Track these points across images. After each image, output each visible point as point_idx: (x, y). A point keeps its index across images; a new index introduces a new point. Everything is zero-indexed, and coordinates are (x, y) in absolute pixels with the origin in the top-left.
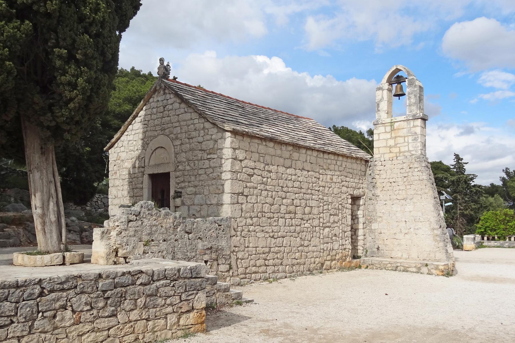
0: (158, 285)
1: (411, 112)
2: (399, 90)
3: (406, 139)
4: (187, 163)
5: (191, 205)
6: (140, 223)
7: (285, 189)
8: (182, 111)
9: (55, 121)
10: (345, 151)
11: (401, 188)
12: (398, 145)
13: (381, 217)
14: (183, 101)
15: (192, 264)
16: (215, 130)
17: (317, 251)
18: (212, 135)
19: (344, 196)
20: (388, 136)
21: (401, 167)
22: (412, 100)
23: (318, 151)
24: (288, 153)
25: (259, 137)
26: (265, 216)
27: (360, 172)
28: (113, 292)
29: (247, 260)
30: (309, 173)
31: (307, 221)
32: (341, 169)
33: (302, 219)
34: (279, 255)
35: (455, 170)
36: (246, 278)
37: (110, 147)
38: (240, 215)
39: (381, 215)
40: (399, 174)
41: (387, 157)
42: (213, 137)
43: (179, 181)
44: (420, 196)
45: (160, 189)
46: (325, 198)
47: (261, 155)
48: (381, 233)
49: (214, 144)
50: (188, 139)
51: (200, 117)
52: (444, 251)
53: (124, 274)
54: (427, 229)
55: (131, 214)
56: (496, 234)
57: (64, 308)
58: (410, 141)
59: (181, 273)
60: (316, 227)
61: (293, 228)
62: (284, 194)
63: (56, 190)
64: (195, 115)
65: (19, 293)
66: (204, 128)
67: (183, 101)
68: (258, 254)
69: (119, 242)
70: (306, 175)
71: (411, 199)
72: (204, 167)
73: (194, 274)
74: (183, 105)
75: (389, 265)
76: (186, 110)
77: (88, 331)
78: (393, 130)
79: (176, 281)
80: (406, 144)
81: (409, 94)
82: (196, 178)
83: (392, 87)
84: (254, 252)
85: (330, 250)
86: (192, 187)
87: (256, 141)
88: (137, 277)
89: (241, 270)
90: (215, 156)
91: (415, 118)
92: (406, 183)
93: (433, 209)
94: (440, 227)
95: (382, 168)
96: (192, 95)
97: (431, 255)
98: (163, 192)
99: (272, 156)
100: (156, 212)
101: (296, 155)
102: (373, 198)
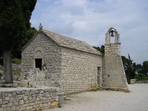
7: (78, 65)
10: (96, 53)
51: (52, 42)
56: (141, 79)
57: (22, 99)
87: (70, 50)
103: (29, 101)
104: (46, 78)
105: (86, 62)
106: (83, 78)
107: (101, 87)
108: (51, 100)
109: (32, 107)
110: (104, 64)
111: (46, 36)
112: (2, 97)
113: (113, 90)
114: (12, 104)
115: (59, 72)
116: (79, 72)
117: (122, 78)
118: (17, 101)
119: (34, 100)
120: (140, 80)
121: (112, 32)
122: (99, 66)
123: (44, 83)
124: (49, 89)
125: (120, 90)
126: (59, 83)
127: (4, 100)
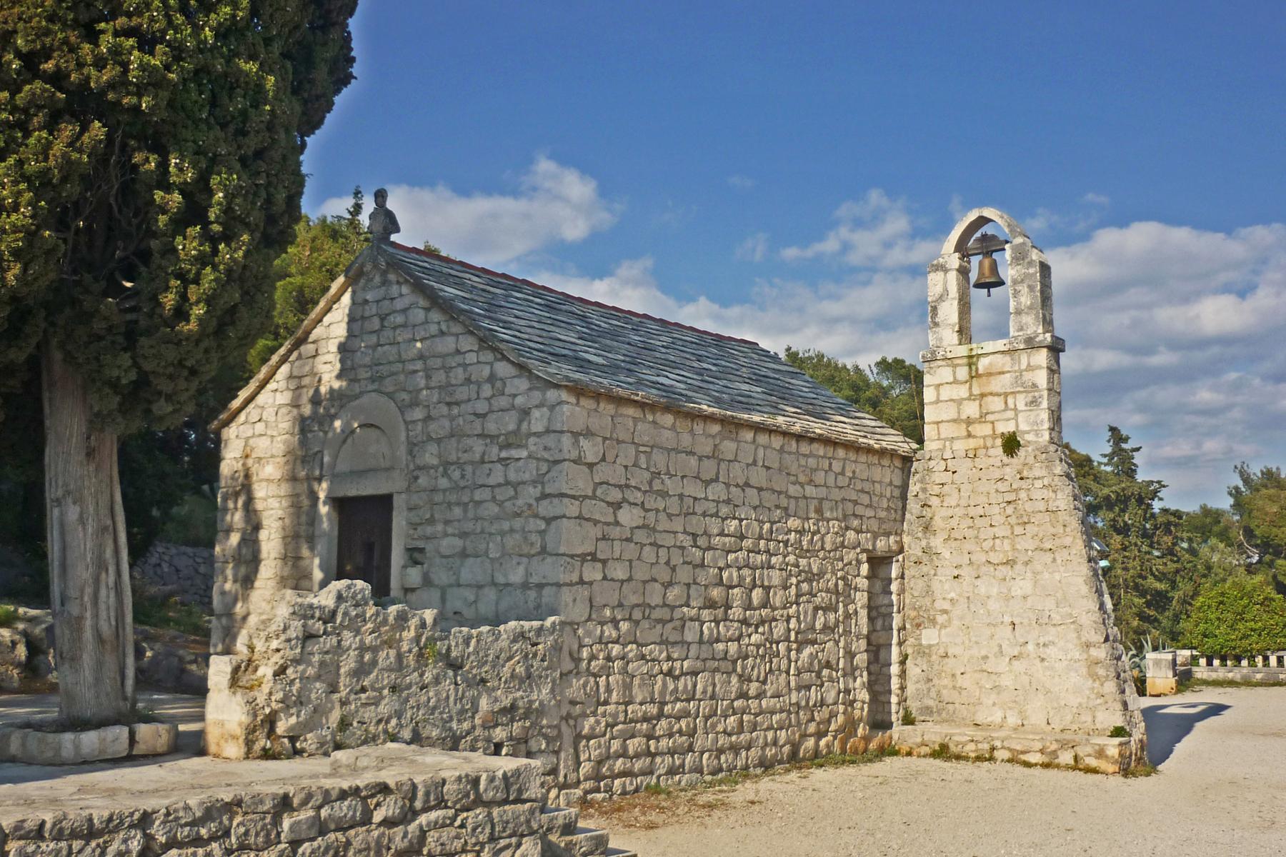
0: (424, 823)
1: (1021, 329)
2: (987, 271)
3: (1010, 401)
4: (441, 469)
5: (451, 586)
6: (335, 640)
8: (433, 329)
9: (139, 368)
11: (1000, 532)
12: (990, 418)
13: (945, 612)
14: (435, 301)
15: (505, 764)
16: (523, 384)
17: (782, 711)
18: (515, 396)
19: (850, 556)
20: (963, 392)
21: (998, 475)
22: (1023, 299)
24: (710, 441)
25: (636, 401)
26: (649, 617)
27: (889, 489)
28: (315, 844)
29: (602, 740)
31: (757, 627)
32: (842, 481)
33: (744, 622)
34: (683, 723)
35: (1109, 469)
36: (598, 790)
37: (227, 423)
38: (586, 615)
39: (946, 606)
40: (993, 494)
41: (960, 446)
42: (519, 401)
43: (417, 520)
44: (1049, 554)
45: (361, 538)
46: (803, 562)
47: (642, 449)
48: (946, 656)
49: (521, 421)
50: (449, 404)
52: (1119, 706)
53: (343, 795)
54: (1070, 646)
58: (1021, 406)
59: (482, 787)
60: (778, 643)
61: (721, 646)
62: (698, 553)
63: (117, 551)
64: (468, 343)
65: (94, 851)
66: (492, 378)
67: (435, 301)
68: (632, 721)
69: (280, 695)
71: (1026, 563)
72: (491, 481)
73: (511, 789)
74: (435, 316)
75: (971, 746)
76: (444, 328)
78: (974, 376)
79: (468, 810)
80: (1010, 414)
81: (1015, 282)
82: (465, 511)
83: (969, 262)
84: (621, 718)
85: (815, 705)
86: (454, 535)
88: (375, 801)
89: (586, 768)
90: (524, 454)
91: (1031, 344)
92: (1013, 520)
93: (1085, 589)
94: (1107, 639)
95: (947, 477)
96: (460, 284)
97: (1083, 718)
98: (369, 548)
99: (669, 451)
100: (374, 609)
101: (728, 447)
102: (925, 559)
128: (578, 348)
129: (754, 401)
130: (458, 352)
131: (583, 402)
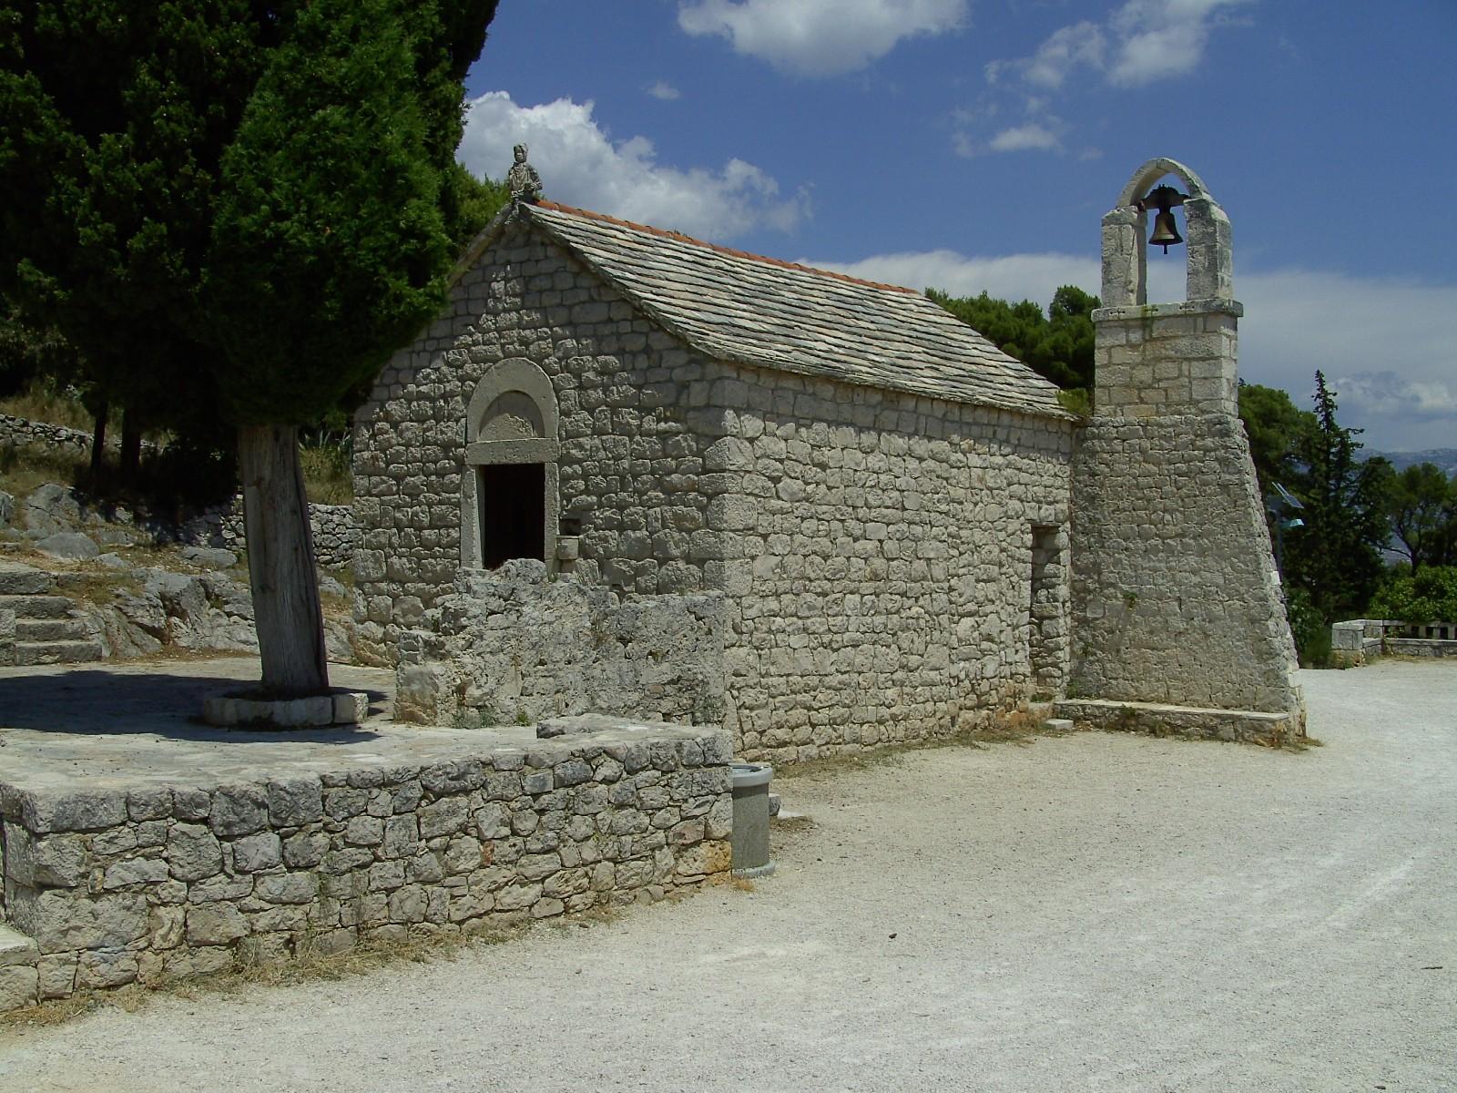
7: (862, 513)
8: (583, 296)
19: (1014, 525)
20: (1135, 356)
23: (947, 401)
30: (924, 464)
42: (678, 374)
46: (963, 533)
49: (679, 394)
55: (494, 595)
57: (464, 829)
66: (647, 350)
70: (915, 470)
77: (506, 884)
79: (672, 772)
103: (519, 841)
104: (599, 641)
105: (928, 486)
106: (905, 629)
107: (1060, 700)
108: (678, 828)
109: (538, 887)
110: (1084, 499)
111: (575, 268)
112: (327, 819)
113: (1157, 728)
114: (400, 871)
115: (704, 583)
116: (875, 577)
117: (1253, 621)
118: (436, 843)
119: (550, 834)
120: (1422, 630)
121: (1164, 199)
122: (1047, 513)
123: (581, 685)
124: (662, 741)
125: (1230, 729)
126: (705, 683)
127: (340, 843)
128: (734, 313)
129: (915, 364)
130: (610, 320)
131: (744, 376)
